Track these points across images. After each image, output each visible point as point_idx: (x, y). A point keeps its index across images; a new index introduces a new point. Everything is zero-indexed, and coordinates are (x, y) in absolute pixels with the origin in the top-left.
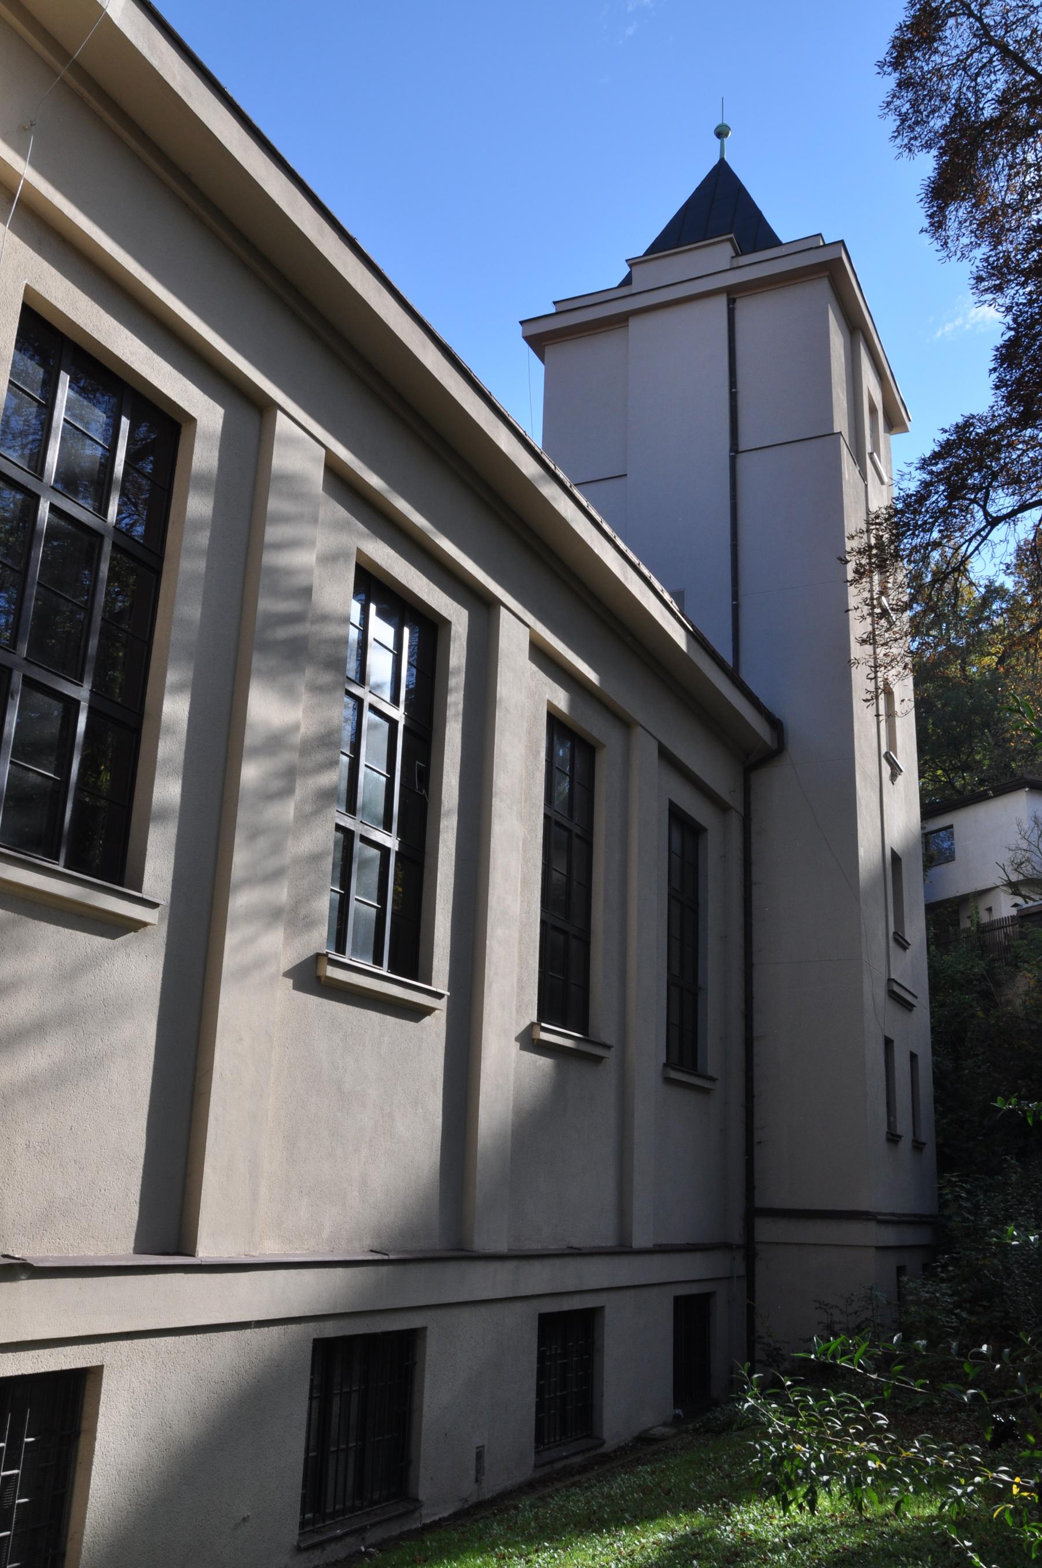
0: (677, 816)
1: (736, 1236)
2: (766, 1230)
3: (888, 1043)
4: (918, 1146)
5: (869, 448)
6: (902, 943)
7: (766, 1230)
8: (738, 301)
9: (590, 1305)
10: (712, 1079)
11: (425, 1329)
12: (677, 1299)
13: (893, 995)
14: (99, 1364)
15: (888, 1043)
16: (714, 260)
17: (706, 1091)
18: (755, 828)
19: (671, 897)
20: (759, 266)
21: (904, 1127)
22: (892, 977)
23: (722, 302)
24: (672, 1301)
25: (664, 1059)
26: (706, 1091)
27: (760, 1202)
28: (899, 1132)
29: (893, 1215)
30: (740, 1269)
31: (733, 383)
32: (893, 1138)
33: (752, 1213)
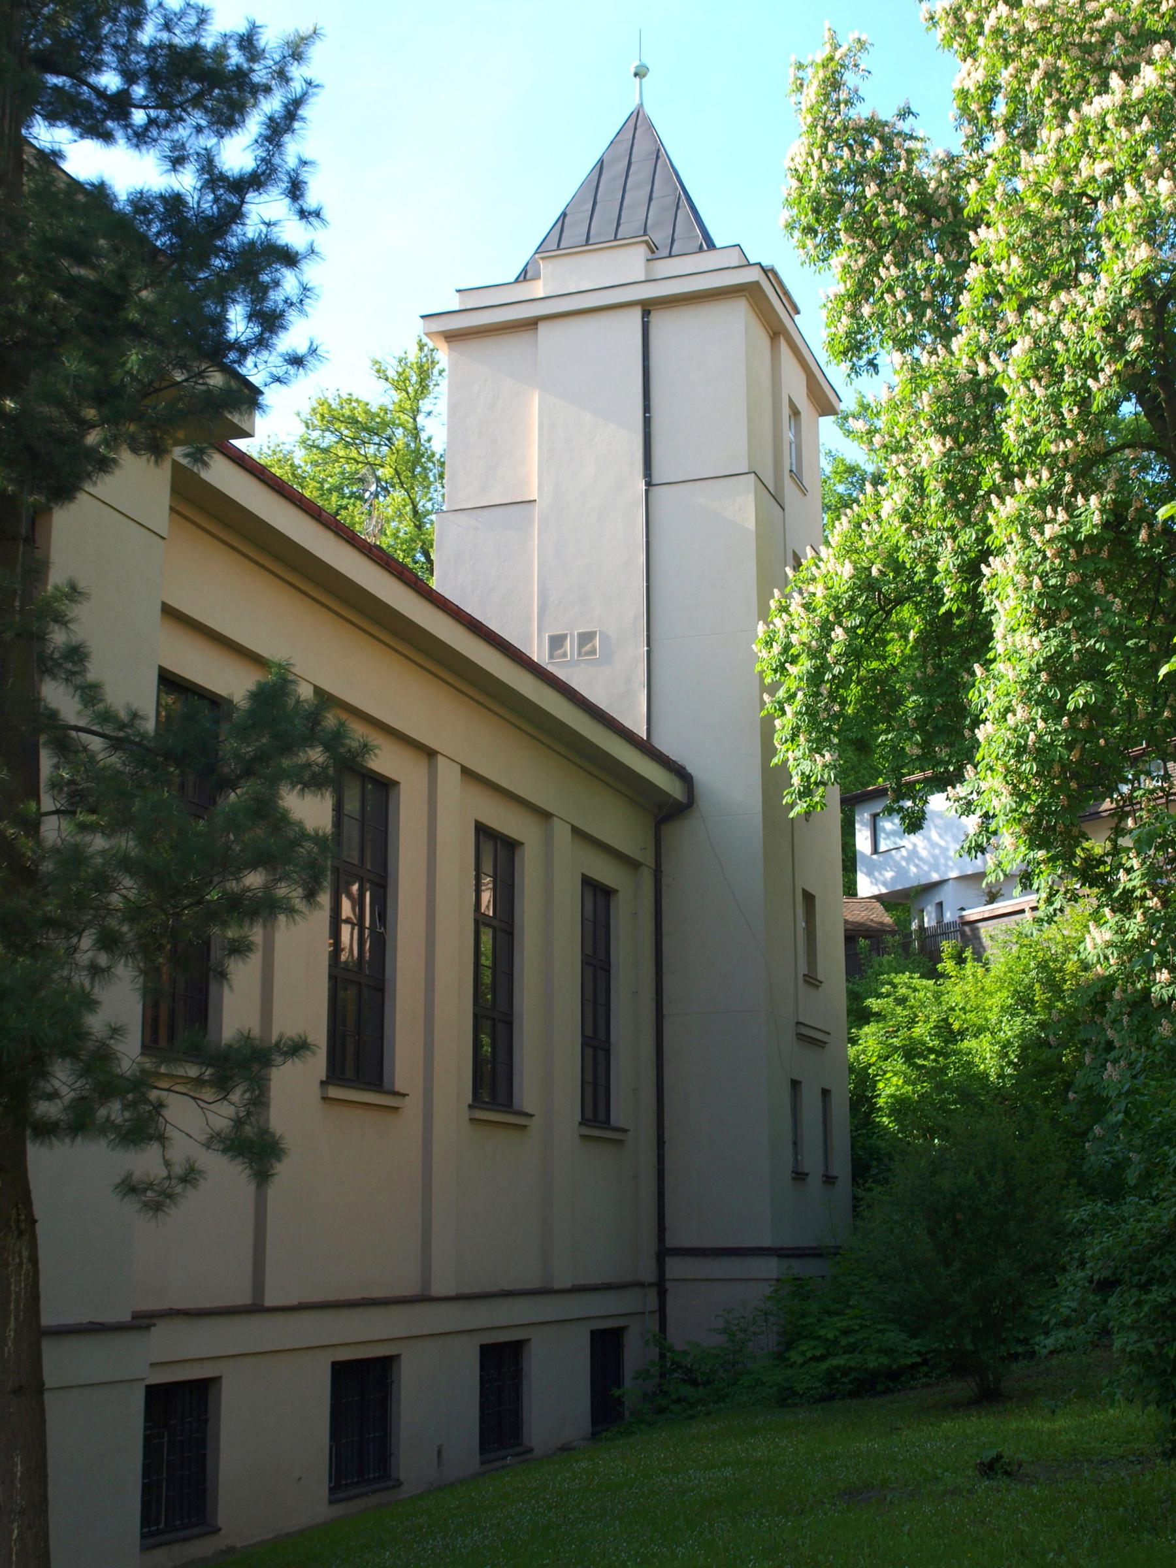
0: (588, 883)
1: (648, 1273)
2: (676, 1268)
3: (825, 1093)
4: (829, 1180)
5: (793, 446)
6: (812, 981)
7: (676, 1268)
8: (652, 313)
9: (388, 1353)
10: (624, 1131)
11: (398, 1356)
12: (335, 1365)
13: (801, 1037)
14: (217, 1374)
15: (825, 1093)
16: (623, 269)
17: (621, 1142)
18: (665, 881)
19: (585, 963)
20: (685, 272)
21: (813, 1163)
22: (801, 1020)
23: (637, 314)
24: (329, 1368)
25: (578, 1118)
26: (621, 1142)
27: (670, 1243)
28: (835, 1174)
29: (798, 1248)
30: (652, 1302)
31: (647, 408)
32: (800, 1176)
33: (663, 1253)
